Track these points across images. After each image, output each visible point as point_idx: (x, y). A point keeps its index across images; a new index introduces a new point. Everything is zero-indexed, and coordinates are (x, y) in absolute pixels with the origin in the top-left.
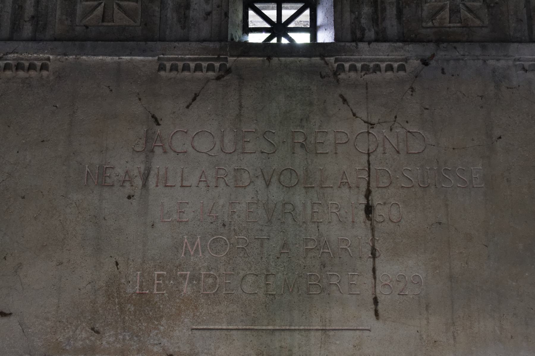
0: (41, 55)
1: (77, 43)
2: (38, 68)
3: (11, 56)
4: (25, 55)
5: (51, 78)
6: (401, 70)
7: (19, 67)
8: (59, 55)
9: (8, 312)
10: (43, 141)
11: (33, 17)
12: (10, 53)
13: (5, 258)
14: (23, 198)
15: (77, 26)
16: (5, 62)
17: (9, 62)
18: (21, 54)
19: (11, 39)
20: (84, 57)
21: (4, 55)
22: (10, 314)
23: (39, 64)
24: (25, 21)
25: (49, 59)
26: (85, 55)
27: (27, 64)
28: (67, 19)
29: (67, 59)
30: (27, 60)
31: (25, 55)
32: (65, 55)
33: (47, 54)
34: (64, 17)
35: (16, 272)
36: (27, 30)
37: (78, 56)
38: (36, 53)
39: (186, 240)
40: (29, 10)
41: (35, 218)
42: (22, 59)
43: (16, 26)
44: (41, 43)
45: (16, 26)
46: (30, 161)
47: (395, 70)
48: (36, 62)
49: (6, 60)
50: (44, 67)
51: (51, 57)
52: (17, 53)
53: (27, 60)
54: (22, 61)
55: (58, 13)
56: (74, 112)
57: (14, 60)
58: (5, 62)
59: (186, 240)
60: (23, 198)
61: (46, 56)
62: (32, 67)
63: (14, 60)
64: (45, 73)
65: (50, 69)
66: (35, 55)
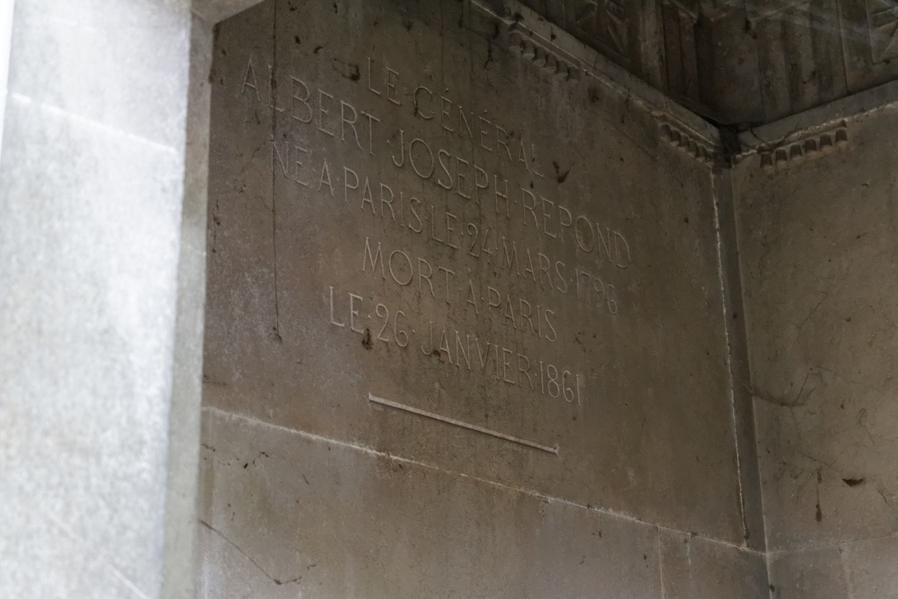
0: (832, 122)
1: (874, 89)
2: (833, 140)
3: (795, 135)
4: (811, 129)
5: (853, 149)
6: (796, 154)
7: (810, 146)
8: (855, 114)
9: (858, 478)
10: (858, 237)
11: (814, 73)
12: (792, 132)
13: (842, 406)
14: (849, 320)
15: (873, 64)
16: (790, 145)
17: (794, 144)
18: (807, 129)
19: (791, 113)
20: (889, 106)
21: (786, 137)
22: (861, 480)
23: (832, 134)
24: (805, 83)
25: (843, 124)
26: (888, 102)
27: (817, 139)
28: (859, 60)
29: (867, 116)
30: (815, 134)
31: (811, 129)
32: (863, 111)
33: (838, 117)
34: (855, 59)
35: (860, 422)
36: (810, 92)
37: (881, 107)
38: (825, 122)
39: (379, 248)
40: (807, 65)
41: (870, 344)
42: (809, 135)
43: (795, 93)
44: (828, 106)
45: (795, 93)
46: (848, 269)
47: (833, 140)
48: (828, 133)
49: (790, 142)
50: (841, 136)
51: (846, 120)
52: (801, 129)
53: (815, 134)
54: (810, 138)
55: (846, 55)
56: (891, 186)
57: (799, 139)
58: (790, 145)
59: (379, 248)
60: (849, 320)
61: (839, 120)
62: (826, 141)
63: (799, 139)
64: (842, 144)
65: (848, 136)
66: (825, 124)
